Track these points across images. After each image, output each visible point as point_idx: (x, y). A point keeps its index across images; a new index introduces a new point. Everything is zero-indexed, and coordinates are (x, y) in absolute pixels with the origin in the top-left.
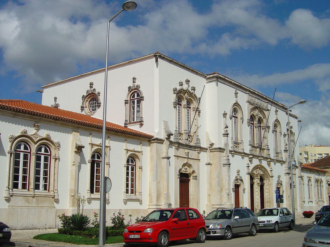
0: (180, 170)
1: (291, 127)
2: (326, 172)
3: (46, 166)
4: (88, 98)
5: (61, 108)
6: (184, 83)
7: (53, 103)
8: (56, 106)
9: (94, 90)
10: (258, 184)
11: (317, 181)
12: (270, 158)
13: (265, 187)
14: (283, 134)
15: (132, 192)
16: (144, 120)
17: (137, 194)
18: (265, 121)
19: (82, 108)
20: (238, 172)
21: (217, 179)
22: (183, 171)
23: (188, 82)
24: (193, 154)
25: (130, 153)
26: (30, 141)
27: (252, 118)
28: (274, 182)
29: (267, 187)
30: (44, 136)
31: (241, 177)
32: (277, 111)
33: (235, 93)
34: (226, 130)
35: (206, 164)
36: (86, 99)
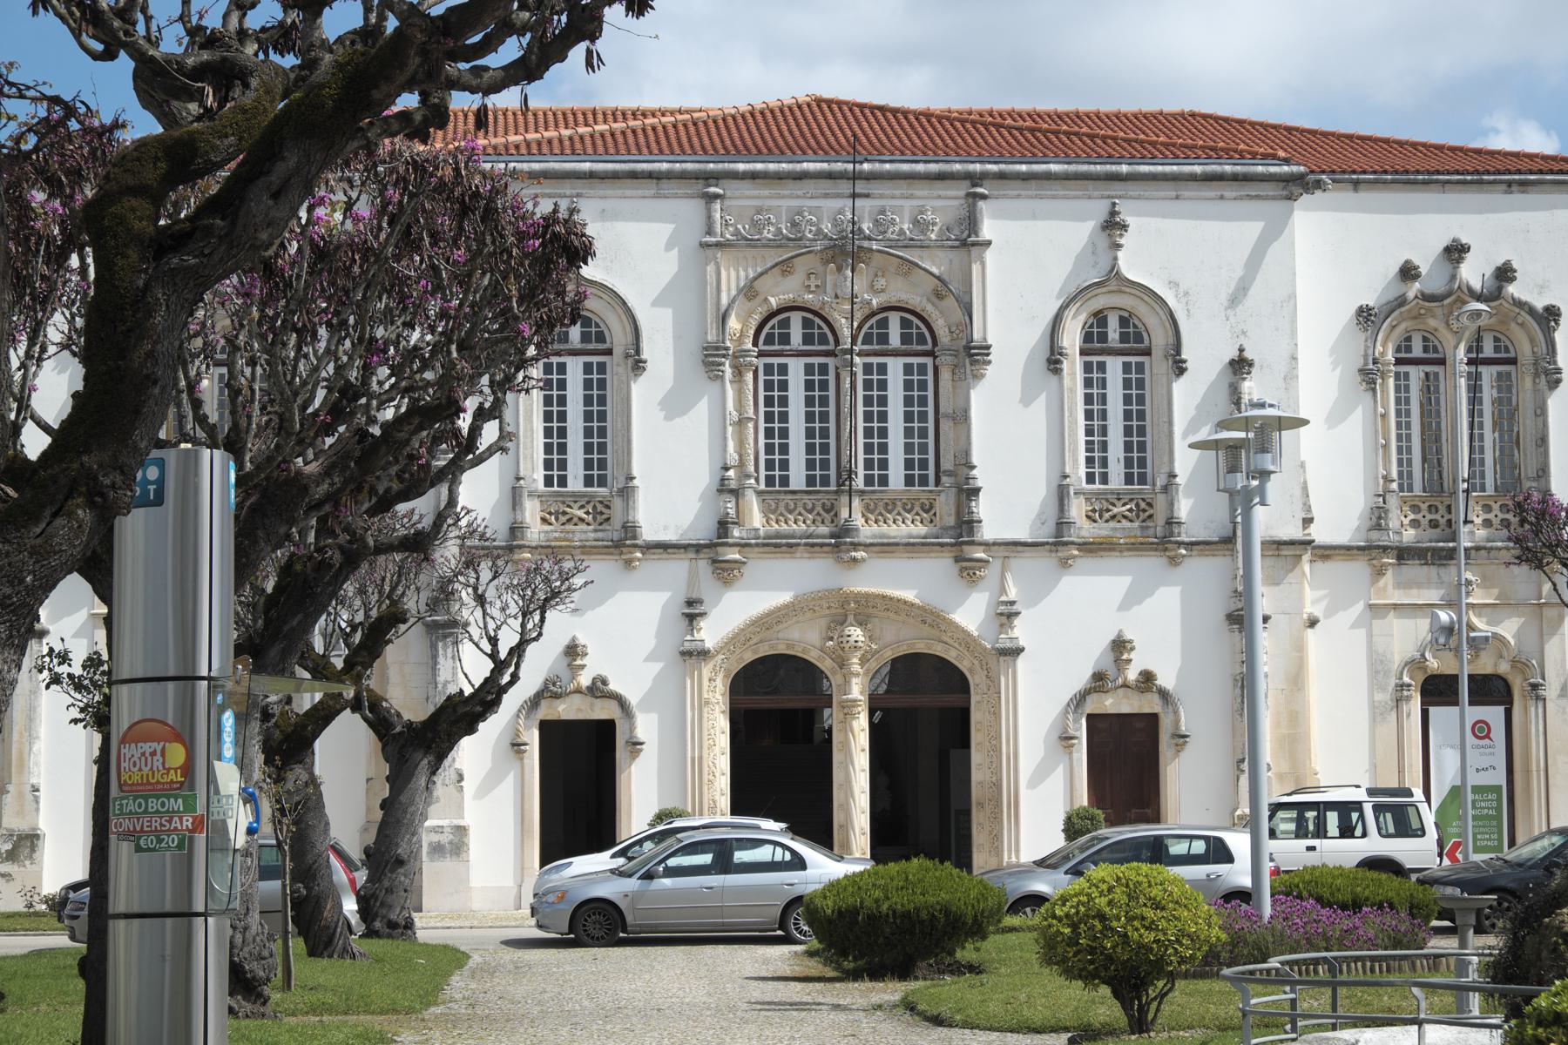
23: (1455, 252)
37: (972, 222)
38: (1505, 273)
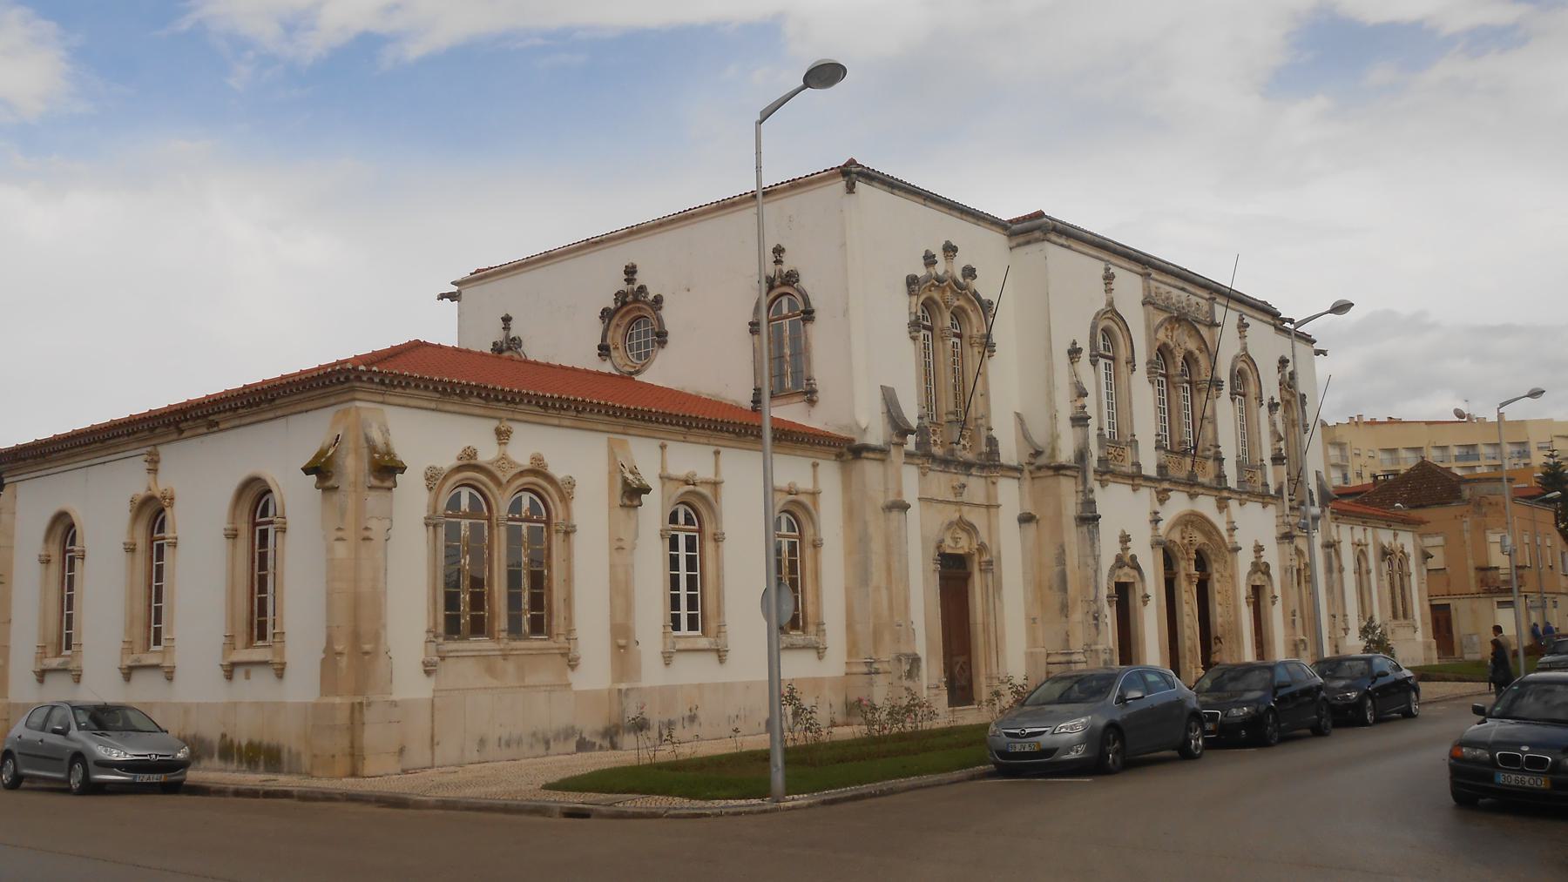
2: (1421, 522)
5: (534, 351)
6: (940, 257)
7: (499, 335)
9: (642, 289)
10: (1189, 576)
11: (1385, 554)
12: (1229, 489)
13: (1216, 586)
14: (1265, 403)
15: (692, 625)
17: (811, 628)
18: (1203, 361)
19: (604, 350)
21: (1057, 569)
23: (950, 250)
24: (976, 487)
26: (491, 485)
27: (1163, 352)
28: (1245, 561)
29: (1217, 586)
30: (525, 462)
31: (1133, 558)
32: (1243, 326)
33: (1105, 278)
35: (442, 297)
36: (614, 322)
37: (1212, 312)
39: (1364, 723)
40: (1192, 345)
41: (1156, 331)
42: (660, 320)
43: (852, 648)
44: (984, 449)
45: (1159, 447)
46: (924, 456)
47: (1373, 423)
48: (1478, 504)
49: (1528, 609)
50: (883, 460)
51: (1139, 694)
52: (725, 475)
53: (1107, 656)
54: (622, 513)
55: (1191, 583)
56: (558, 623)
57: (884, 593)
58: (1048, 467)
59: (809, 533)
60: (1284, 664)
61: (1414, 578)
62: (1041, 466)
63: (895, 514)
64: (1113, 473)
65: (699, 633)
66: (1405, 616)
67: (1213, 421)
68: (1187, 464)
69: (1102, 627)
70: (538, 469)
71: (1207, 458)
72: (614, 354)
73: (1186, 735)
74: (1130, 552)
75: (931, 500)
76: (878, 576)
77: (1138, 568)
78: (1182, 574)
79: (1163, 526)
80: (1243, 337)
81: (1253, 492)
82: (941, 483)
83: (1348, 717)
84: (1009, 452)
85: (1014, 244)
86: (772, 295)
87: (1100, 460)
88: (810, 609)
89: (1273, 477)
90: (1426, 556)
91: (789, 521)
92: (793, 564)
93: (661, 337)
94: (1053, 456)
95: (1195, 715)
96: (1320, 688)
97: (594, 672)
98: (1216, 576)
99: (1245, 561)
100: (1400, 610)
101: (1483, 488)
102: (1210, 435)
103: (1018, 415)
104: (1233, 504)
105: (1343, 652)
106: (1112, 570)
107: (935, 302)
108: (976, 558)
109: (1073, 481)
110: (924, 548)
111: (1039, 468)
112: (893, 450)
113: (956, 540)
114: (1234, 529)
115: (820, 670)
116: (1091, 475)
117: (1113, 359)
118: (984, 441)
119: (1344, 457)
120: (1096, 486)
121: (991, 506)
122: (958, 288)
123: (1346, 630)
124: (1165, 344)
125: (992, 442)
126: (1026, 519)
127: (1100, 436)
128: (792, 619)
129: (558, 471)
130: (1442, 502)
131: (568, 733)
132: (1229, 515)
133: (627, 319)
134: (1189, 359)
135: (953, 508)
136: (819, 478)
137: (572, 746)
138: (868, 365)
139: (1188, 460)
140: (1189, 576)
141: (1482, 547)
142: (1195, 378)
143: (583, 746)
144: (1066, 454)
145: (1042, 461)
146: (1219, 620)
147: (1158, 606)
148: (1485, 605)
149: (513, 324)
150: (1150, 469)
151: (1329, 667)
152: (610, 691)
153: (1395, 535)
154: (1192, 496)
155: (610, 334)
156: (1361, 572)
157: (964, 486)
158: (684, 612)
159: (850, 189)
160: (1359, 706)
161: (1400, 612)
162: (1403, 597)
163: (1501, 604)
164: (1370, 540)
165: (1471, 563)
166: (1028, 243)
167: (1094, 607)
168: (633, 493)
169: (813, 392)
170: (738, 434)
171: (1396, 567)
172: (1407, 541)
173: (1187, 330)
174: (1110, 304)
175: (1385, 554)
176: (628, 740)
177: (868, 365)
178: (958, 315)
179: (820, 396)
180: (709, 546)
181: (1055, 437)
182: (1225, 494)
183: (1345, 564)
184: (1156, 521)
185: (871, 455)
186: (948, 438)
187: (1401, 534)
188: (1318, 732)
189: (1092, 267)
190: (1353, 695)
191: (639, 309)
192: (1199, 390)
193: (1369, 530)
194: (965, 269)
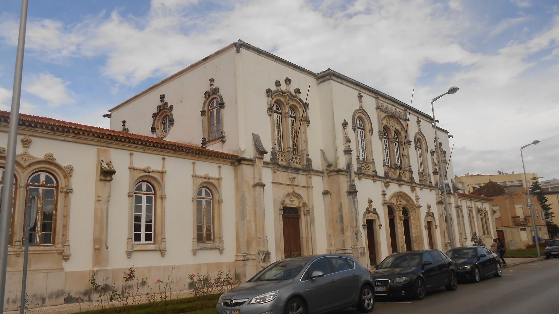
0: (283, 203)
1: (441, 144)
3: (149, 209)
4: (160, 116)
8: (126, 130)
9: (166, 103)
10: (400, 217)
11: (479, 211)
12: (415, 183)
13: (412, 221)
14: (429, 151)
16: (226, 135)
17: (217, 240)
18: (403, 134)
19: (153, 130)
20: (370, 201)
21: (339, 214)
22: (288, 204)
23: (288, 81)
24: (301, 179)
25: (200, 181)
26: (57, 170)
27: (386, 129)
28: (423, 212)
29: (412, 221)
30: (41, 156)
31: (374, 209)
34: (347, 145)
35: (104, 116)
36: (157, 118)
37: (406, 115)
38: (298, 91)
39: (476, 282)
40: (398, 127)
41: (382, 120)
42: (172, 115)
43: (238, 249)
44: (305, 163)
45: (384, 165)
46: (274, 163)
47: (472, 176)
48: (511, 195)
49: (531, 231)
50: (253, 165)
51: (320, 273)
52: (167, 169)
53: (362, 251)
54: (101, 184)
55: (401, 220)
56: (59, 238)
57: (253, 224)
58: (334, 171)
59: (216, 197)
60: (427, 251)
61: (490, 220)
62: (332, 170)
63: (258, 188)
64: (364, 175)
65: (152, 242)
66: (488, 234)
67: (408, 156)
68: (397, 172)
69: (359, 238)
70: (49, 161)
71: (406, 171)
72: (157, 131)
73: (360, 298)
74: (373, 207)
75: (278, 183)
76: (250, 216)
77: (376, 213)
78: (397, 217)
79: (387, 197)
80: (419, 126)
81: (425, 184)
82: (283, 176)
83: (466, 278)
84: (317, 164)
85: (319, 82)
86: (209, 99)
87: (358, 169)
88: (216, 231)
89: (433, 179)
90: (494, 212)
91: (206, 191)
92: (208, 211)
93: (172, 122)
94: (336, 166)
95: (368, 284)
96: (450, 264)
97: (80, 261)
98: (412, 218)
99: (423, 212)
100: (486, 231)
101: (512, 189)
102: (407, 162)
103: (322, 150)
104: (418, 189)
105: (465, 245)
106: (365, 215)
107: (282, 102)
108: (302, 209)
109: (345, 177)
110: (275, 204)
111: (331, 172)
112: (257, 161)
113: (292, 201)
114: (418, 199)
115: (223, 258)
116: (353, 175)
117: (364, 129)
118: (305, 160)
119: (463, 186)
120: (356, 179)
121: (309, 187)
122: (292, 97)
123: (466, 239)
124: (386, 126)
125: (309, 160)
126: (325, 193)
127: (358, 159)
128: (205, 235)
129: (63, 162)
130: (498, 194)
131: (58, 295)
132: (416, 193)
133: (162, 117)
134: (397, 132)
135: (290, 187)
136: (226, 174)
137: (61, 300)
138: (249, 124)
139: (398, 171)
140: (400, 217)
141: (513, 210)
142: (400, 140)
143: (69, 300)
144: (342, 165)
145: (332, 168)
146: (414, 235)
147: (386, 229)
148: (516, 230)
149: (126, 124)
150: (381, 172)
151: (457, 253)
152: (90, 271)
153: (482, 204)
154: (400, 185)
155: (156, 123)
156: (470, 218)
157: (294, 178)
158: (143, 233)
159: (238, 51)
160: (471, 272)
161: (486, 232)
162: (487, 227)
163: (522, 230)
164: (473, 206)
165: (510, 215)
166: (324, 81)
167: (355, 230)
168: (107, 174)
169: (223, 137)
170: (175, 150)
171: (483, 216)
172: (487, 206)
173: (396, 121)
174: (361, 107)
175: (479, 211)
176: (95, 296)
177: (249, 124)
178: (293, 108)
179: (227, 139)
180: (159, 201)
181: (337, 159)
182: (414, 185)
183: (464, 215)
184: (384, 194)
185: (246, 162)
186: (289, 159)
187: (484, 204)
188: (450, 288)
189: (354, 93)
190: (468, 267)
191: (166, 112)
192: (402, 145)
193: (473, 202)
194: (295, 89)
